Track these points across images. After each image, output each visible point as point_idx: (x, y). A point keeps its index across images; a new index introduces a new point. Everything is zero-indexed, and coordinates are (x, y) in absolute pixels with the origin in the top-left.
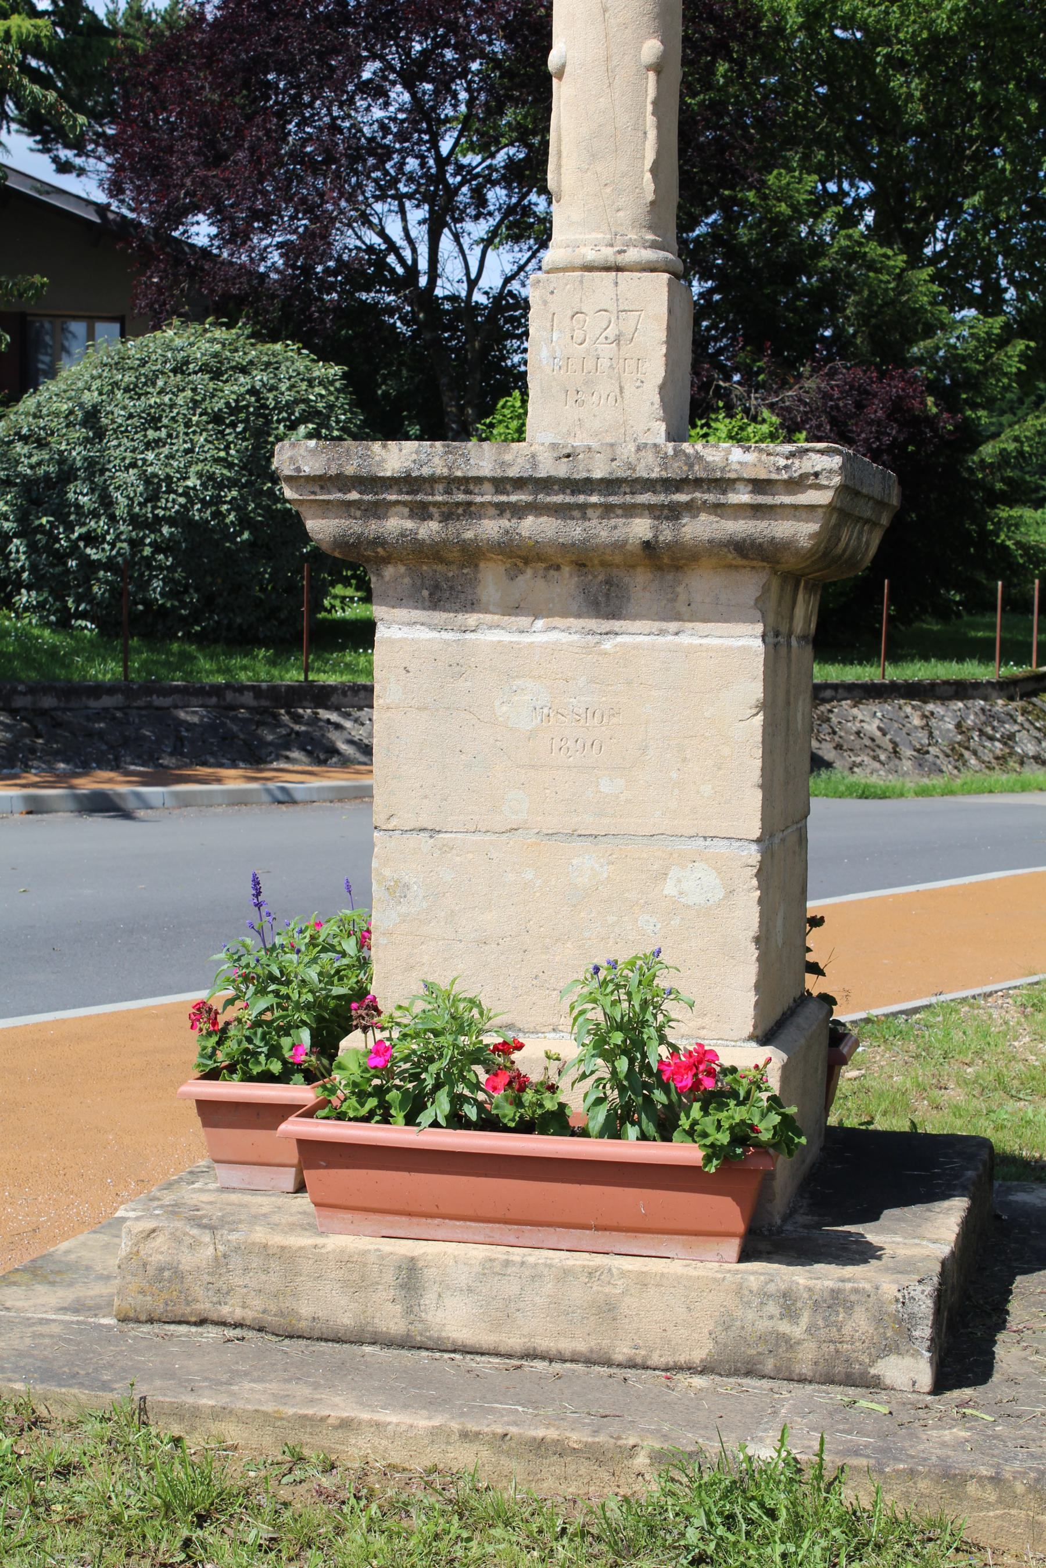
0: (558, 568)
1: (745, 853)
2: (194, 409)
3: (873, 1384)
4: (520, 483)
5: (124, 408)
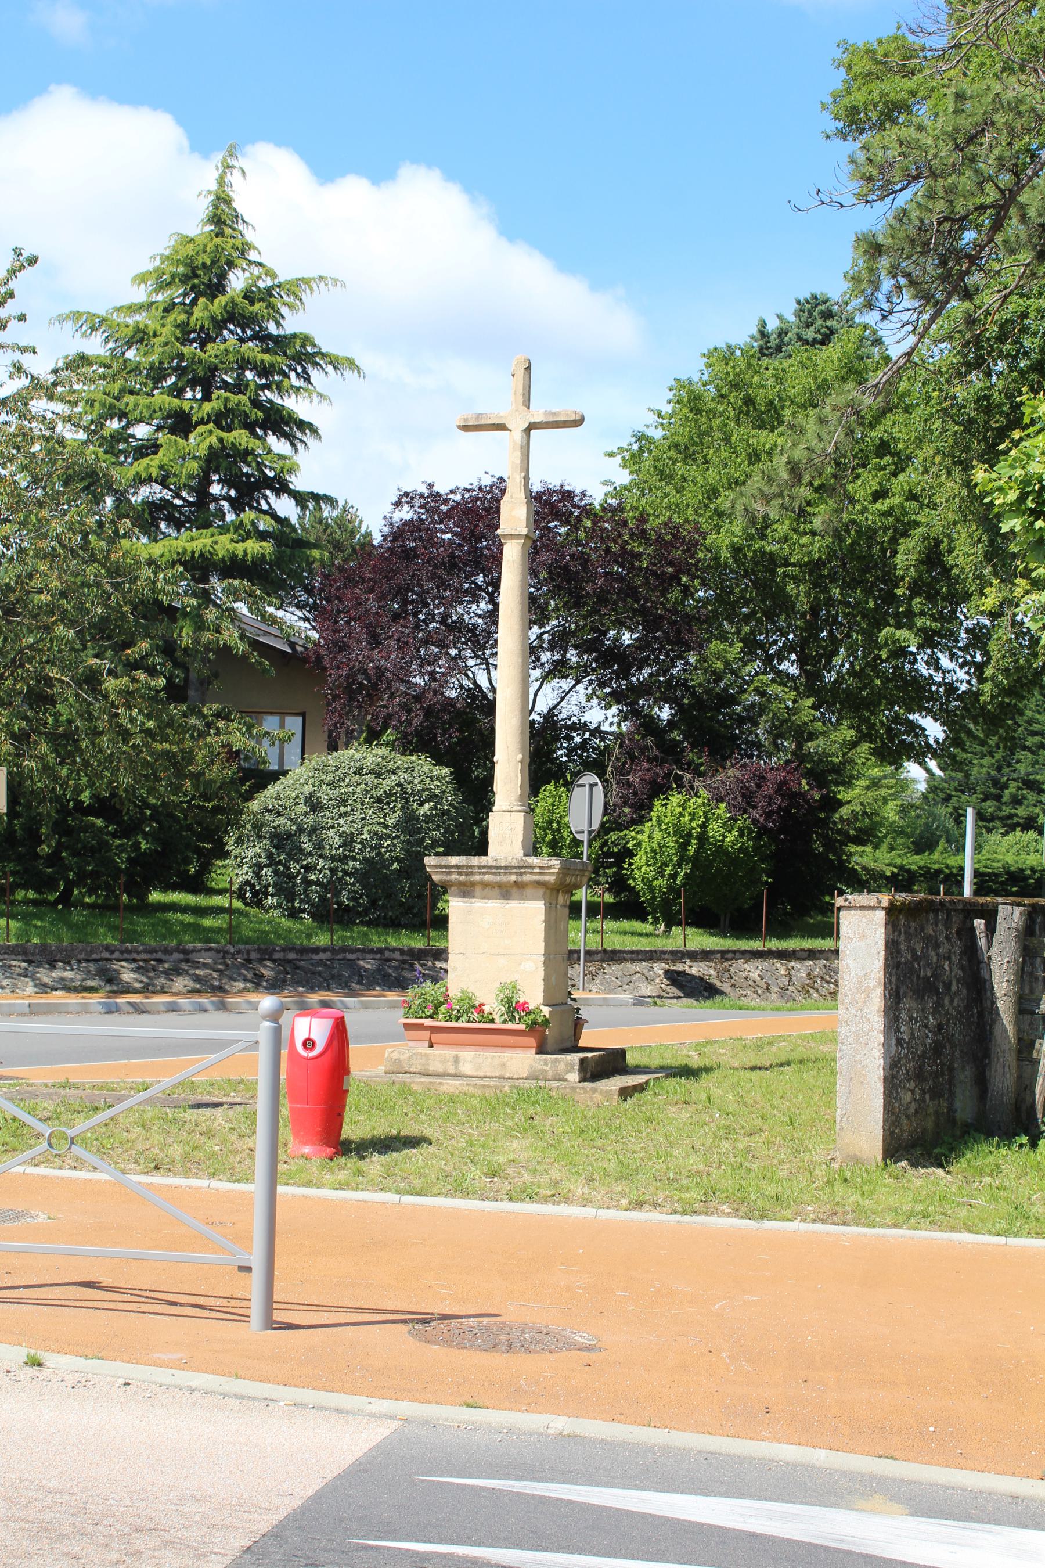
3: (566, 1080)
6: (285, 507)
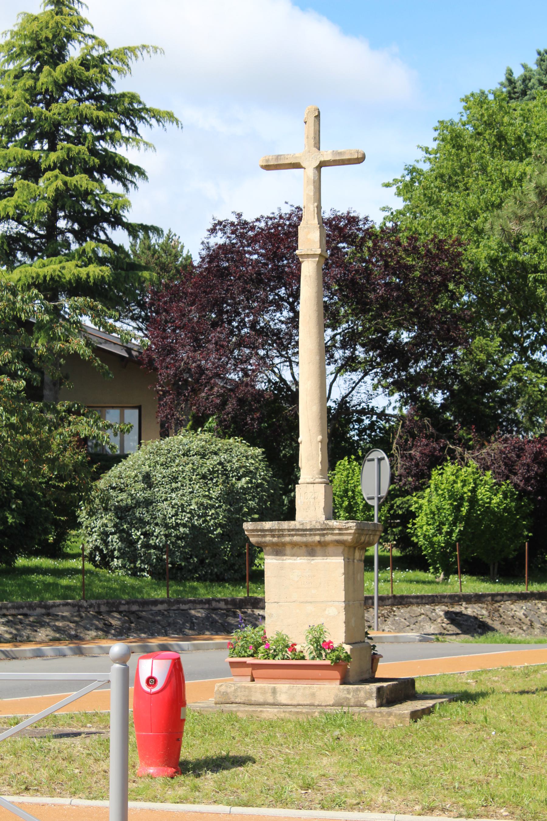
2: (193, 473)
3: (365, 706)
4: (293, 530)
5: (161, 473)
6: (120, 237)
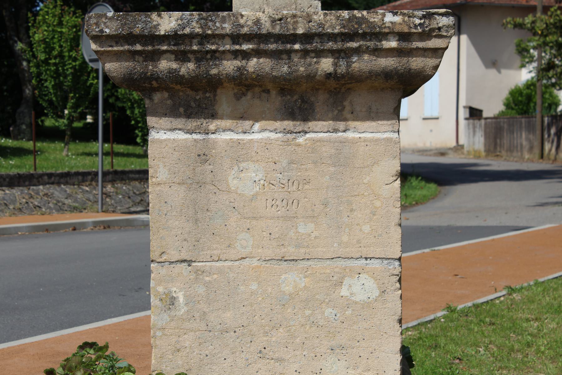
0: (268, 92)
1: (392, 267)
4: (248, 38)
